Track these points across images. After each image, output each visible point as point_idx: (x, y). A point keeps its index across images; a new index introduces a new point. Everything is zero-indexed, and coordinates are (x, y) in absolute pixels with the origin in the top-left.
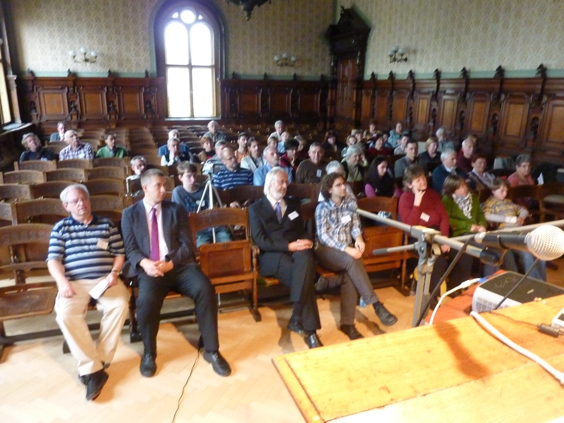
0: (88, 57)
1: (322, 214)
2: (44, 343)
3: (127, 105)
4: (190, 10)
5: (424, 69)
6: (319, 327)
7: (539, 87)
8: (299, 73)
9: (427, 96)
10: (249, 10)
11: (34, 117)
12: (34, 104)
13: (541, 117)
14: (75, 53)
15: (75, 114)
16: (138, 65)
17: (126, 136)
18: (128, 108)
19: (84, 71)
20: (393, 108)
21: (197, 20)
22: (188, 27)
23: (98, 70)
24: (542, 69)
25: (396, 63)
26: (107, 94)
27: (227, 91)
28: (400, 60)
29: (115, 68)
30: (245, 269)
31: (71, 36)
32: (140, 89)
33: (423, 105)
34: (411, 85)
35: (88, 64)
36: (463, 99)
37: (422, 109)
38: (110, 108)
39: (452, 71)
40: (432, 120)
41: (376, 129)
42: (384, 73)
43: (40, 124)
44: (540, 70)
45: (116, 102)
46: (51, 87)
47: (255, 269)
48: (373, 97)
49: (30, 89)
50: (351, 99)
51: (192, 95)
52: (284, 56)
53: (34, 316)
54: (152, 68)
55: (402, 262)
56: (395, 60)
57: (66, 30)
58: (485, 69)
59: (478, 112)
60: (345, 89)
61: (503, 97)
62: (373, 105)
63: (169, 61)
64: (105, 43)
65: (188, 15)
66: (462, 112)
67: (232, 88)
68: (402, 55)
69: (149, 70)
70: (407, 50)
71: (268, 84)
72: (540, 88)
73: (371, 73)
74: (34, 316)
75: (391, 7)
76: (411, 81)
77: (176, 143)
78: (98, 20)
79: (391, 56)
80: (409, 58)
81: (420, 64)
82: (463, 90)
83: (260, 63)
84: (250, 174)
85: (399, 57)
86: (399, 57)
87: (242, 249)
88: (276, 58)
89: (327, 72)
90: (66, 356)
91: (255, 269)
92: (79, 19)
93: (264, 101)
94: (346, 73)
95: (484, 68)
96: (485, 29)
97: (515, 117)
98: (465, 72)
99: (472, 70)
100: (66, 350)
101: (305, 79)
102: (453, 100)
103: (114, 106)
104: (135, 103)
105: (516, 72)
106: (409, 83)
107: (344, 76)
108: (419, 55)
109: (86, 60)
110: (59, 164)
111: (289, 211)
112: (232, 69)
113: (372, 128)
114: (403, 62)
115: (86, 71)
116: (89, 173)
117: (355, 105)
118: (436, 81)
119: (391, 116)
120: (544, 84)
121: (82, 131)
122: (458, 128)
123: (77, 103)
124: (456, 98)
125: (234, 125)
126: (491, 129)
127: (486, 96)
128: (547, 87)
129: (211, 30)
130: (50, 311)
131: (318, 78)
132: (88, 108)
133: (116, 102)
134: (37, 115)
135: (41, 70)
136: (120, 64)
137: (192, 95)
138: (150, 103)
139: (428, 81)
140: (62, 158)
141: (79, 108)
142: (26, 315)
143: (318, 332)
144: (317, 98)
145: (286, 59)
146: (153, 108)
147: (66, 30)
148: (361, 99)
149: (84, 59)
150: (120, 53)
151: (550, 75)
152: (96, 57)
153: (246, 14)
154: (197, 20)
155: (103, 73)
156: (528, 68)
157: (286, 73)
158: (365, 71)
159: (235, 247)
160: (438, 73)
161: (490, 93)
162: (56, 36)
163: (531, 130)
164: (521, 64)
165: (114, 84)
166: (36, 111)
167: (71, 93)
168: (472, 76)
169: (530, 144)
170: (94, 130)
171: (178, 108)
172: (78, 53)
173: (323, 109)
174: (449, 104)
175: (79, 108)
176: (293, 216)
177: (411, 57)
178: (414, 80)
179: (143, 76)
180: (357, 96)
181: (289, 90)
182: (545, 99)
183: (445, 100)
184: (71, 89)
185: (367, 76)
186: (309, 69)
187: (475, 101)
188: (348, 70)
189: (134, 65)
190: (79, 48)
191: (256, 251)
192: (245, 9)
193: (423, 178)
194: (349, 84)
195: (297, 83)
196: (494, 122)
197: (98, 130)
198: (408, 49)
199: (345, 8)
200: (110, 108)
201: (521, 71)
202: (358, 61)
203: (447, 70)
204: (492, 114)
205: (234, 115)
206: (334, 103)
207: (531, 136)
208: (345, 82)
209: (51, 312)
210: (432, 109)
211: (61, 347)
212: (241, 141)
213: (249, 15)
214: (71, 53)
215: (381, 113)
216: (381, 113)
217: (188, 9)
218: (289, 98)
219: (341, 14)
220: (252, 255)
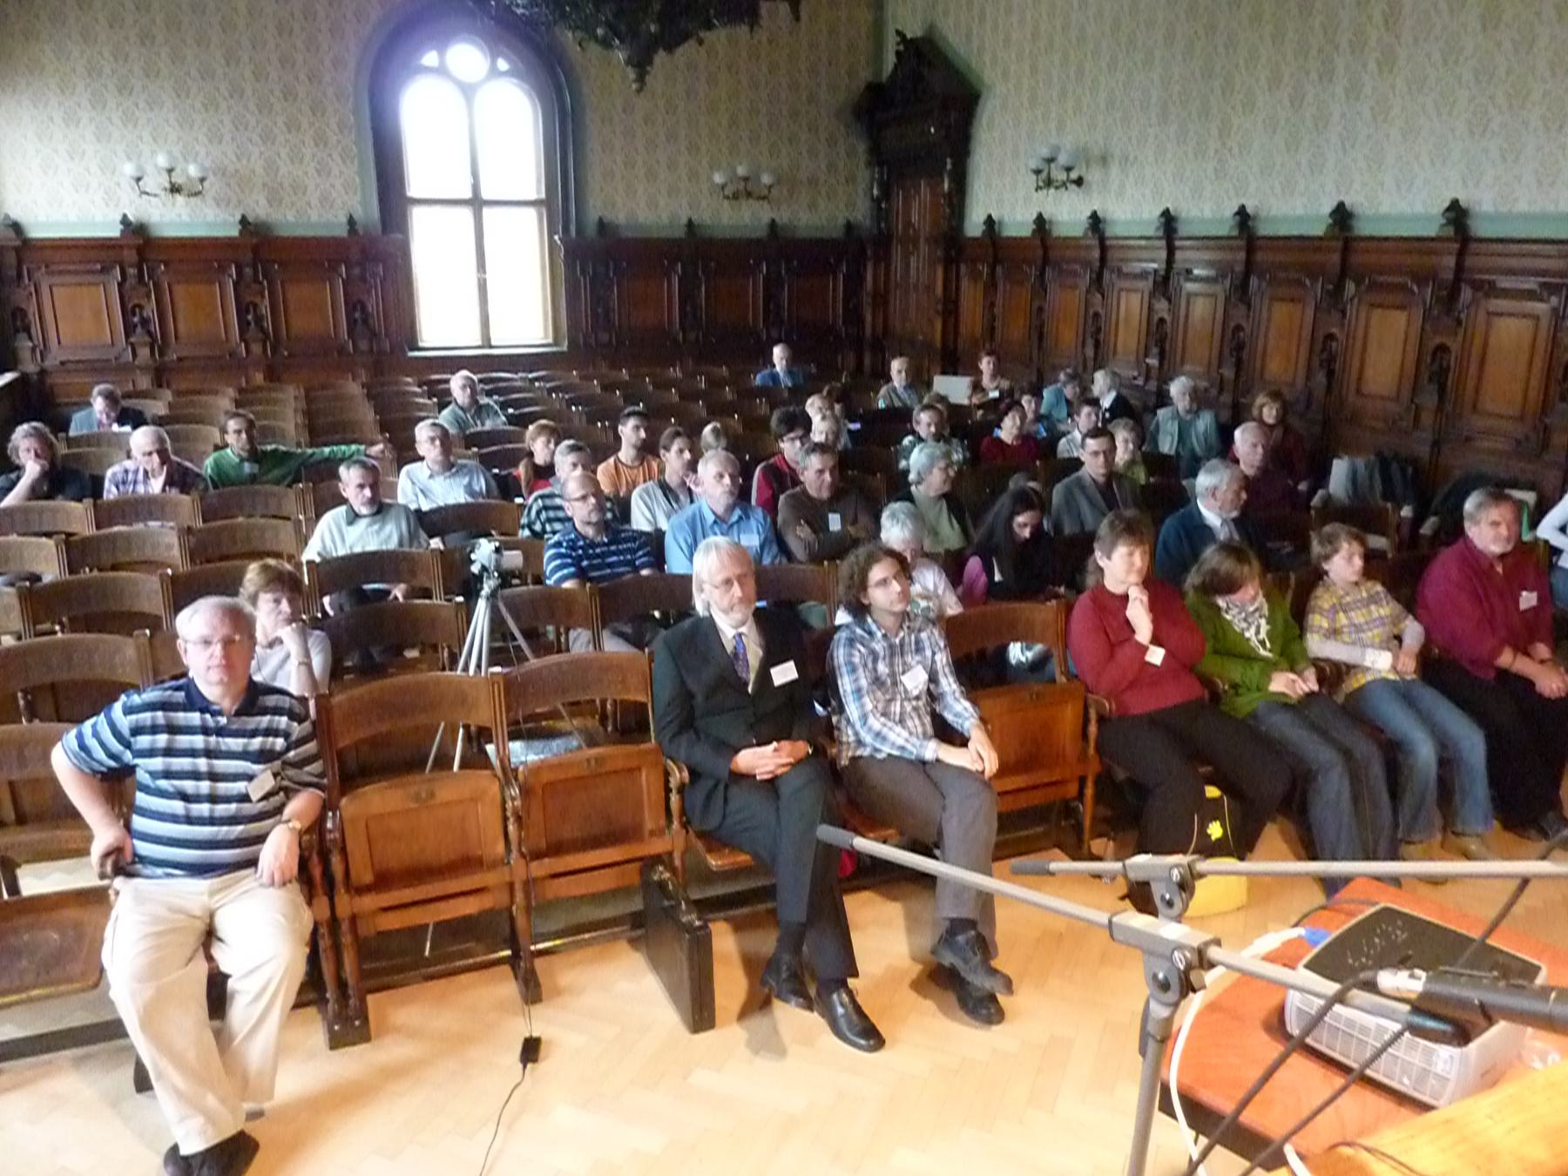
0: (178, 179)
1: (856, 660)
2: (78, 1062)
3: (300, 316)
4: (473, 42)
5: (1130, 209)
6: (855, 974)
7: (1450, 261)
8: (783, 216)
9: (1141, 284)
10: (641, 64)
11: (25, 354)
12: (23, 313)
13: (1454, 346)
14: (140, 167)
15: (145, 344)
16: (325, 200)
17: (296, 411)
18: (302, 324)
19: (167, 219)
20: (1045, 316)
21: (494, 72)
22: (468, 90)
23: (210, 218)
24: (1457, 214)
25: (1052, 191)
26: (236, 285)
27: (583, 271)
28: (1064, 184)
29: (260, 209)
30: (649, 825)
31: (129, 119)
32: (334, 268)
33: (1130, 307)
34: (1096, 254)
35: (180, 199)
36: (1240, 292)
37: (1126, 319)
38: (249, 323)
39: (1208, 214)
40: (1155, 350)
41: (998, 373)
42: (1019, 218)
43: (43, 372)
44: (1451, 215)
45: (265, 307)
46: (71, 267)
47: (676, 825)
48: (991, 286)
49: (13, 273)
50: (930, 288)
51: (483, 280)
52: (741, 171)
53: (47, 997)
54: (366, 208)
55: (1082, 781)
56: (1049, 183)
57: (112, 104)
58: (1300, 211)
59: (1282, 331)
60: (913, 260)
61: (1350, 287)
62: (992, 305)
63: (414, 189)
64: (227, 138)
65: (467, 57)
66: (1238, 328)
67: (598, 264)
68: (1069, 169)
69: (359, 214)
70: (1083, 154)
71: (696, 252)
72: (1453, 265)
73: (983, 218)
74: (47, 997)
75: (1035, 36)
76: (1095, 242)
77: (438, 432)
78: (207, 74)
79: (1038, 172)
80: (1088, 178)
81: (1120, 194)
82: (1239, 268)
83: (673, 191)
84: (655, 543)
85: (1062, 176)
86: (1062, 176)
87: (639, 769)
88: (718, 178)
89: (861, 213)
90: (142, 1098)
91: (676, 825)
92: (150, 72)
93: (687, 297)
94: (915, 218)
95: (1296, 209)
96: (1297, 100)
97: (1385, 346)
98: (1243, 217)
99: (1263, 214)
100: (143, 1083)
101: (802, 233)
102: (1214, 296)
103: (259, 319)
104: (317, 309)
105: (1386, 218)
106: (1088, 247)
107: (908, 224)
108: (1114, 170)
109: (175, 189)
110: (106, 514)
111: (772, 658)
112: (596, 209)
113: (986, 365)
114: (1073, 187)
115: (174, 219)
116: (193, 540)
117: (940, 307)
118: (1163, 243)
119: (1041, 337)
120: (1461, 255)
121: (168, 395)
122: (1228, 373)
123: (150, 310)
124: (1219, 290)
125: (604, 368)
126: (1321, 378)
127: (1304, 285)
128: (1470, 261)
129: (534, 106)
130: (94, 979)
131: (837, 232)
132: (181, 327)
133: (265, 307)
134: (33, 349)
135: (42, 218)
136: (274, 198)
137: (483, 280)
138: (364, 309)
139: (1143, 243)
140: (110, 492)
141: (155, 327)
142: (24, 996)
143: (851, 982)
144: (837, 287)
145: (746, 179)
146: (374, 322)
147: (112, 104)
148: (958, 288)
149: (168, 185)
150: (271, 167)
151: (1481, 228)
152: (202, 180)
153: (631, 74)
154: (494, 72)
155: (225, 223)
156: (1419, 209)
157: (749, 219)
158: (968, 211)
159: (620, 764)
160: (1169, 221)
161: (1314, 280)
162: (85, 120)
163: (1430, 380)
164: (1402, 200)
165: (258, 255)
166: (30, 338)
167: (132, 281)
168: (1264, 230)
169: (1427, 419)
170: (199, 393)
171: (443, 320)
172: (149, 169)
173: (854, 316)
174: (1201, 303)
175: (155, 327)
176: (784, 673)
177: (1093, 176)
178: (1102, 240)
179: (343, 232)
180: (946, 281)
181: (758, 265)
182: (1466, 294)
183: (1189, 295)
184: (132, 271)
185: (974, 226)
186: (812, 206)
187: (1272, 299)
188: (919, 209)
189: (314, 202)
190: (153, 153)
191: (678, 776)
192: (629, 62)
193: (1143, 553)
194: (924, 248)
195: (779, 246)
196: (1327, 357)
197: (216, 393)
198: (1092, 157)
199: (909, 36)
200: (249, 323)
201: (1401, 218)
202: (946, 186)
203: (1195, 213)
204: (1320, 335)
205: (604, 337)
206: (881, 299)
207: (1429, 400)
208: (911, 241)
209: (97, 977)
210: (1156, 318)
211: (129, 1073)
212: (630, 432)
213: (641, 79)
214: (129, 169)
215: (1015, 330)
216: (1015, 330)
217: (465, 40)
218: (755, 289)
219: (898, 53)
220: (667, 782)
